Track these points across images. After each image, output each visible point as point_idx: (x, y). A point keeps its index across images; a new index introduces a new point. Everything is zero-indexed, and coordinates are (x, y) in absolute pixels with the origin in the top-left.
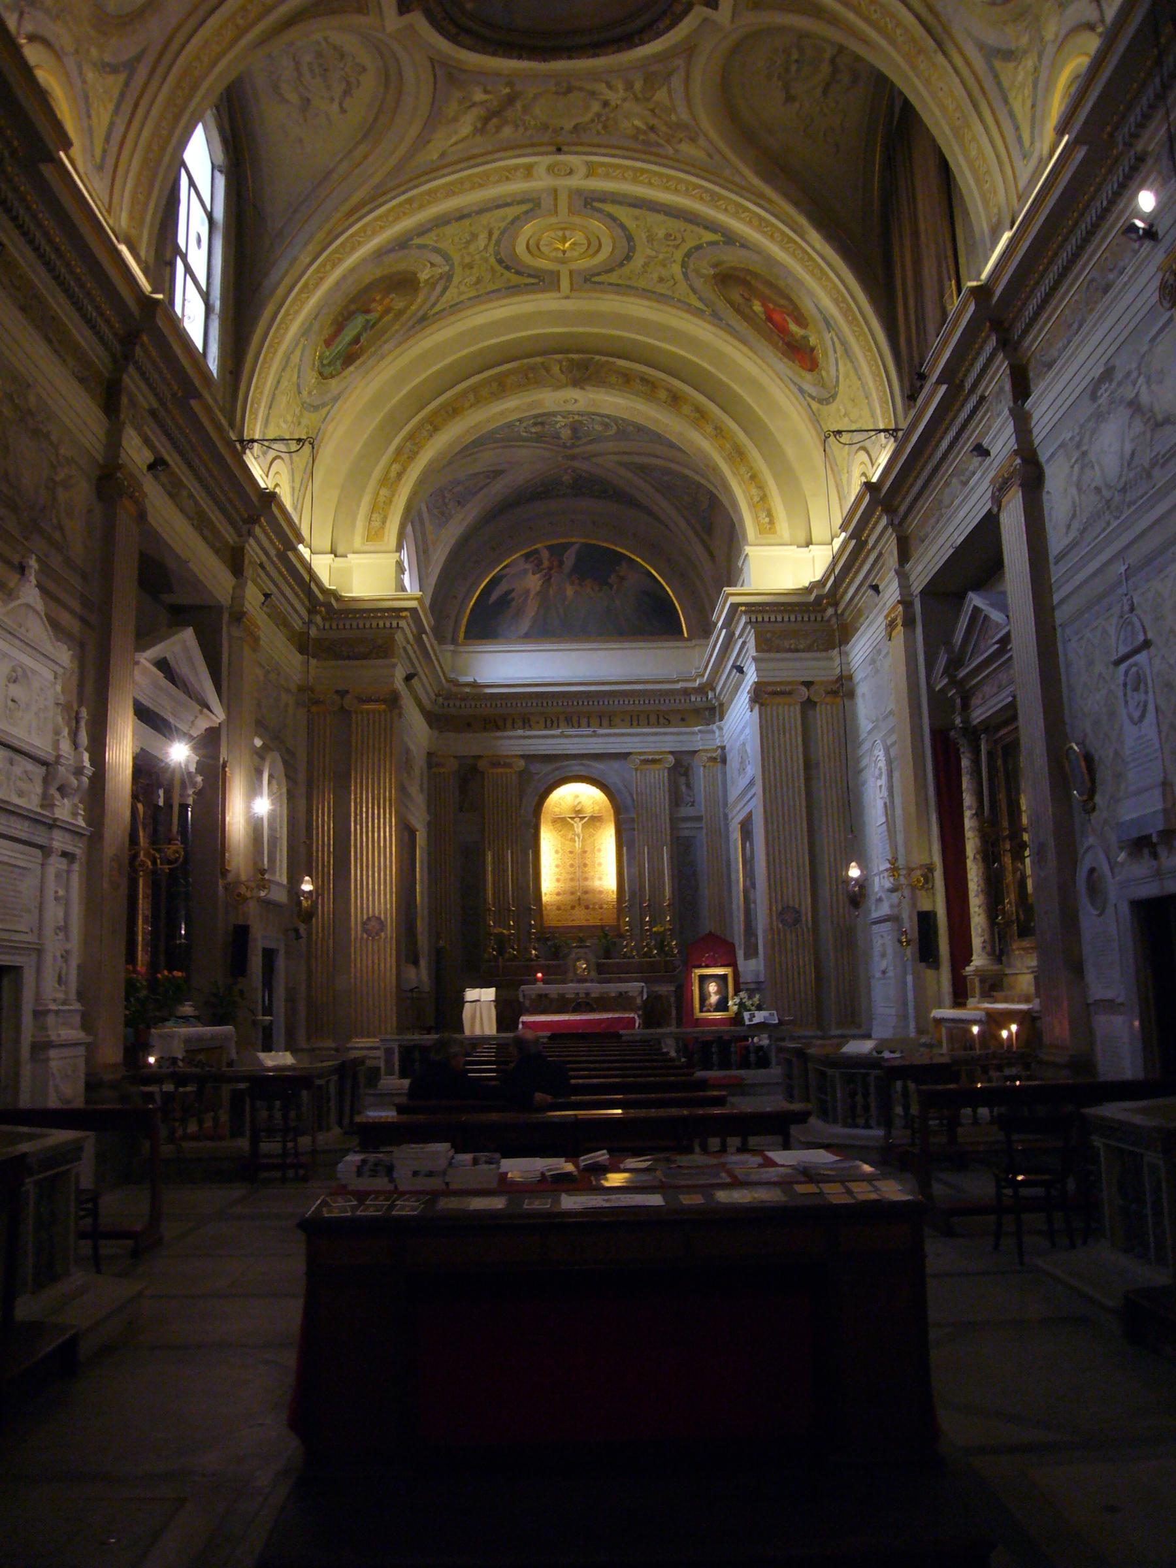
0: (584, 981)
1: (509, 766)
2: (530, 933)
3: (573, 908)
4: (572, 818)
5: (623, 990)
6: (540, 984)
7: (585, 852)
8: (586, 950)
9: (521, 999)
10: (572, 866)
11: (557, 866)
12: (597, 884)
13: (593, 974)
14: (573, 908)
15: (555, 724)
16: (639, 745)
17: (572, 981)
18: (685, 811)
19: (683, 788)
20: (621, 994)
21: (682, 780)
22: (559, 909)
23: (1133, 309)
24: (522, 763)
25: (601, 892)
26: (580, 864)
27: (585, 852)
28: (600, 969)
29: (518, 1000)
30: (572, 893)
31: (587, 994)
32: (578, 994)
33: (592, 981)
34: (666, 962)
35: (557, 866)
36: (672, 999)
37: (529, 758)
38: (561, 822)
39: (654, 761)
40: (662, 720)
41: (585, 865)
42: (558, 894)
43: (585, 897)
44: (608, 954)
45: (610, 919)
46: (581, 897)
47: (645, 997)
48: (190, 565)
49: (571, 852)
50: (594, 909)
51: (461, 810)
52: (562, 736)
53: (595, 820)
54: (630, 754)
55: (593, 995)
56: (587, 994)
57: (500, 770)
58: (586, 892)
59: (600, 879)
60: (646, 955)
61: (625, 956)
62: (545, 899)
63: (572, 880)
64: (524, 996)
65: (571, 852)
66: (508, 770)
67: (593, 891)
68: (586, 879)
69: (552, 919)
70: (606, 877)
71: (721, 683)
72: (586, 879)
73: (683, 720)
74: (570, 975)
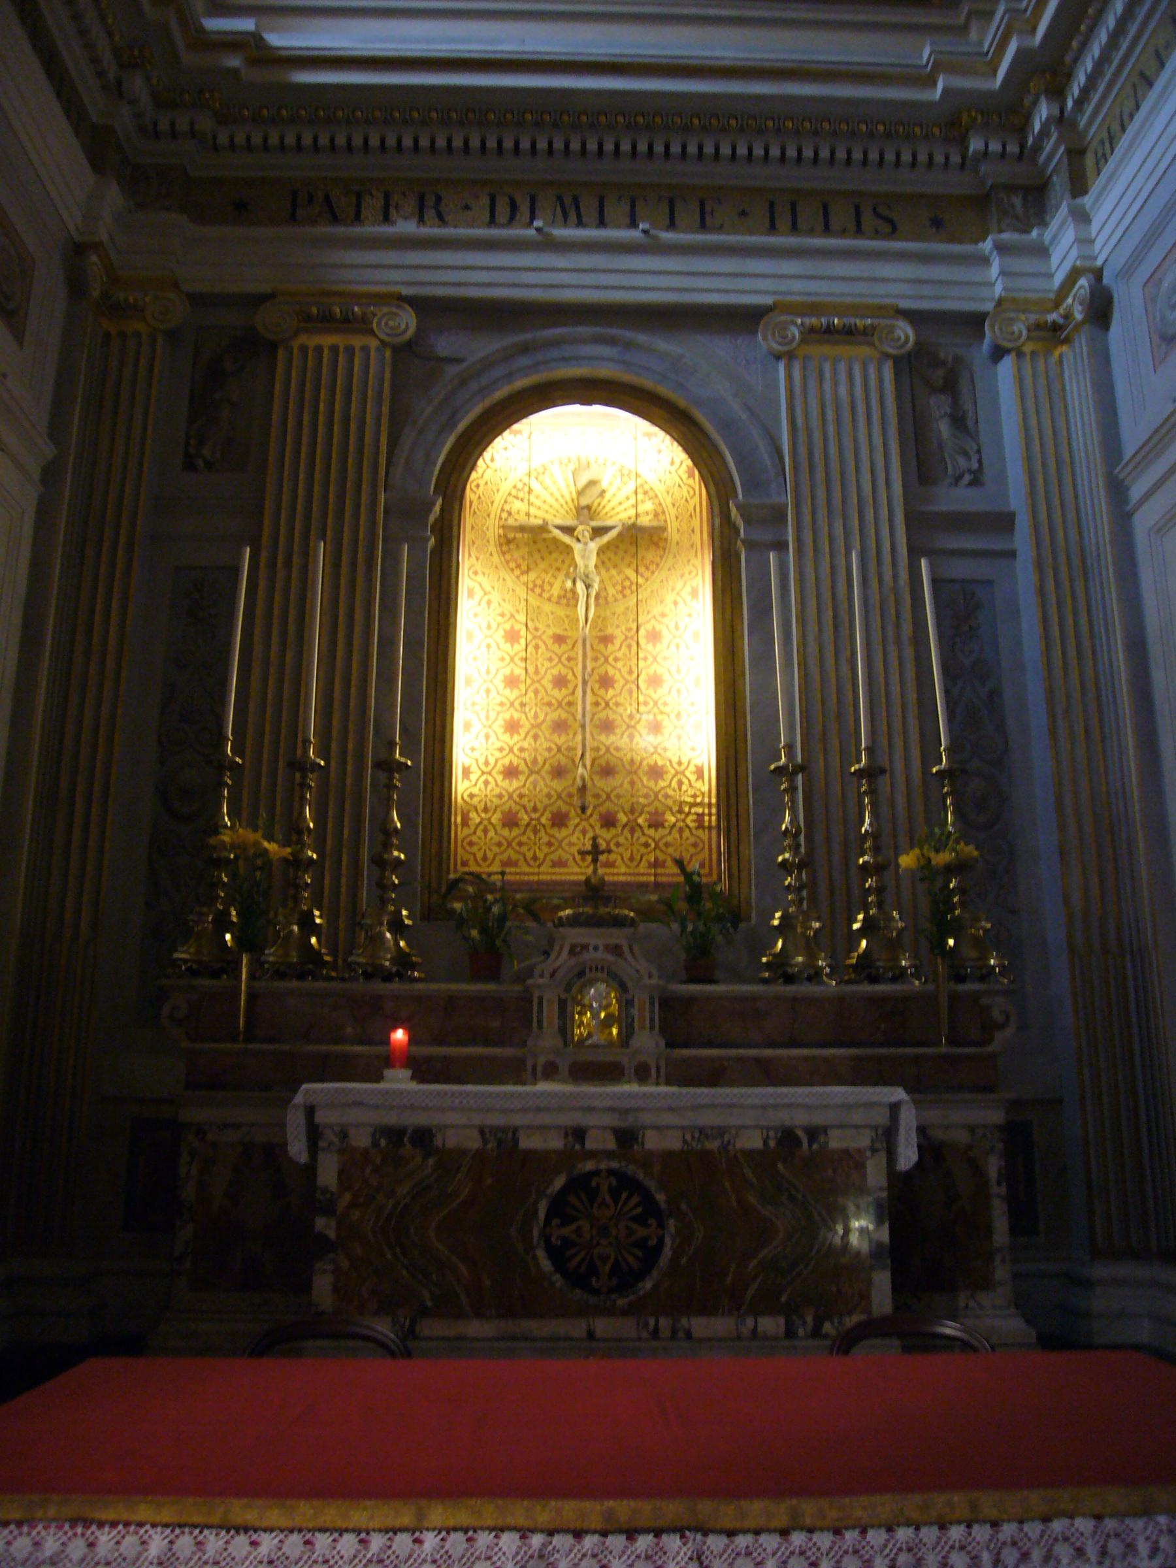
0: (609, 1072)
1: (362, 325)
2: (382, 863)
3: (559, 820)
4: (569, 530)
5: (800, 1119)
6: (399, 1080)
7: (606, 640)
8: (618, 936)
9: (297, 1149)
10: (560, 682)
11: (511, 682)
12: (643, 744)
13: (647, 1042)
14: (559, 820)
15: (524, 208)
16: (798, 286)
17: (550, 1072)
18: (953, 499)
19: (944, 428)
20: (788, 1137)
21: (939, 405)
22: (510, 821)
23: (1088, 497)
24: (408, 321)
25: (656, 772)
26: (586, 672)
27: (606, 640)
28: (676, 1020)
29: (274, 1151)
30: (558, 772)
31: (626, 1137)
32: (579, 1134)
33: (642, 1074)
34: (953, 998)
35: (511, 682)
36: (993, 1166)
37: (425, 307)
38: (533, 545)
39: (849, 333)
40: (868, 219)
41: (606, 682)
42: (510, 772)
43: (600, 783)
44: (700, 963)
45: (705, 855)
46: (586, 787)
47: (908, 1156)
48: (527, 1142)
49: (559, 639)
50: (633, 827)
51: (189, 465)
52: (548, 245)
53: (637, 543)
54: (767, 310)
55: (652, 1142)
56: (626, 1137)
57: (328, 341)
58: (607, 771)
59: (656, 728)
60: (866, 969)
61: (781, 970)
62: (463, 787)
63: (560, 726)
64: (314, 1133)
65: (559, 639)
66: (357, 341)
67: (633, 768)
68: (607, 726)
69: (478, 848)
70: (676, 726)
71: (1088, 64)
72: (607, 726)
73: (937, 223)
74: (546, 1042)
